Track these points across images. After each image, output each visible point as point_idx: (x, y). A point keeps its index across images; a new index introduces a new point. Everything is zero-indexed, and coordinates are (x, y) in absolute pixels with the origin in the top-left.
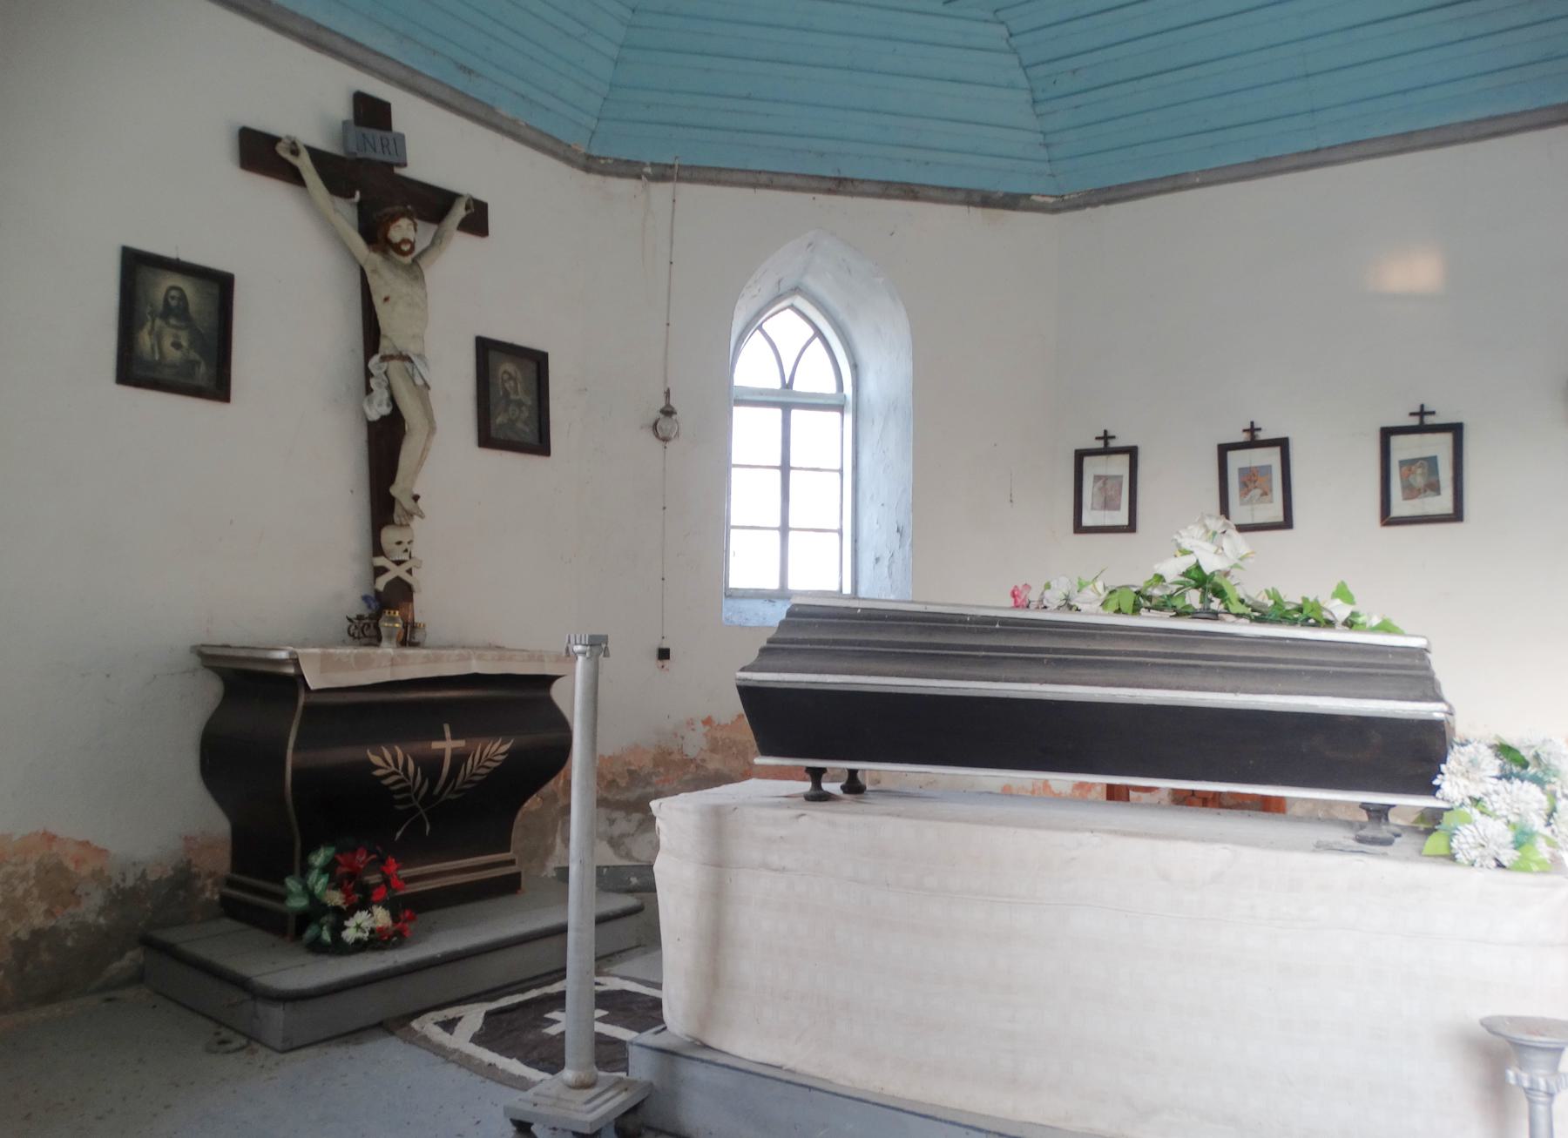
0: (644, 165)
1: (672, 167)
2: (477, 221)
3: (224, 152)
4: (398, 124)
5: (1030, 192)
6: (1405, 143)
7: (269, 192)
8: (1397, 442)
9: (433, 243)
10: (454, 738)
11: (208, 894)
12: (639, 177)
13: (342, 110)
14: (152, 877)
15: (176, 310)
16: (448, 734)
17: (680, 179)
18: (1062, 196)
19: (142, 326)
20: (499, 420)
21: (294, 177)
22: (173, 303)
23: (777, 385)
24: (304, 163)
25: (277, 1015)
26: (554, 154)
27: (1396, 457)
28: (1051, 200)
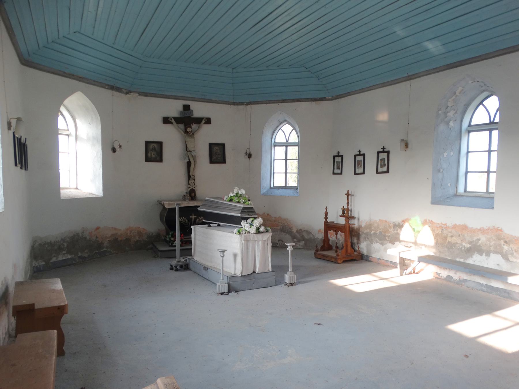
0: (244, 103)
1: (249, 102)
2: (208, 121)
3: (160, 121)
4: (191, 108)
5: (325, 97)
6: (384, 85)
7: (169, 127)
8: (357, 157)
9: (198, 129)
10: (194, 216)
11: (162, 238)
12: (244, 105)
13: (181, 108)
14: (154, 235)
15: (154, 149)
16: (193, 215)
17: (251, 104)
18: (333, 97)
19: (149, 152)
20: (214, 158)
21: (172, 123)
22: (153, 148)
23: (285, 141)
24: (173, 121)
25: (160, 253)
26: (226, 104)
27: (380, 158)
28: (331, 98)
